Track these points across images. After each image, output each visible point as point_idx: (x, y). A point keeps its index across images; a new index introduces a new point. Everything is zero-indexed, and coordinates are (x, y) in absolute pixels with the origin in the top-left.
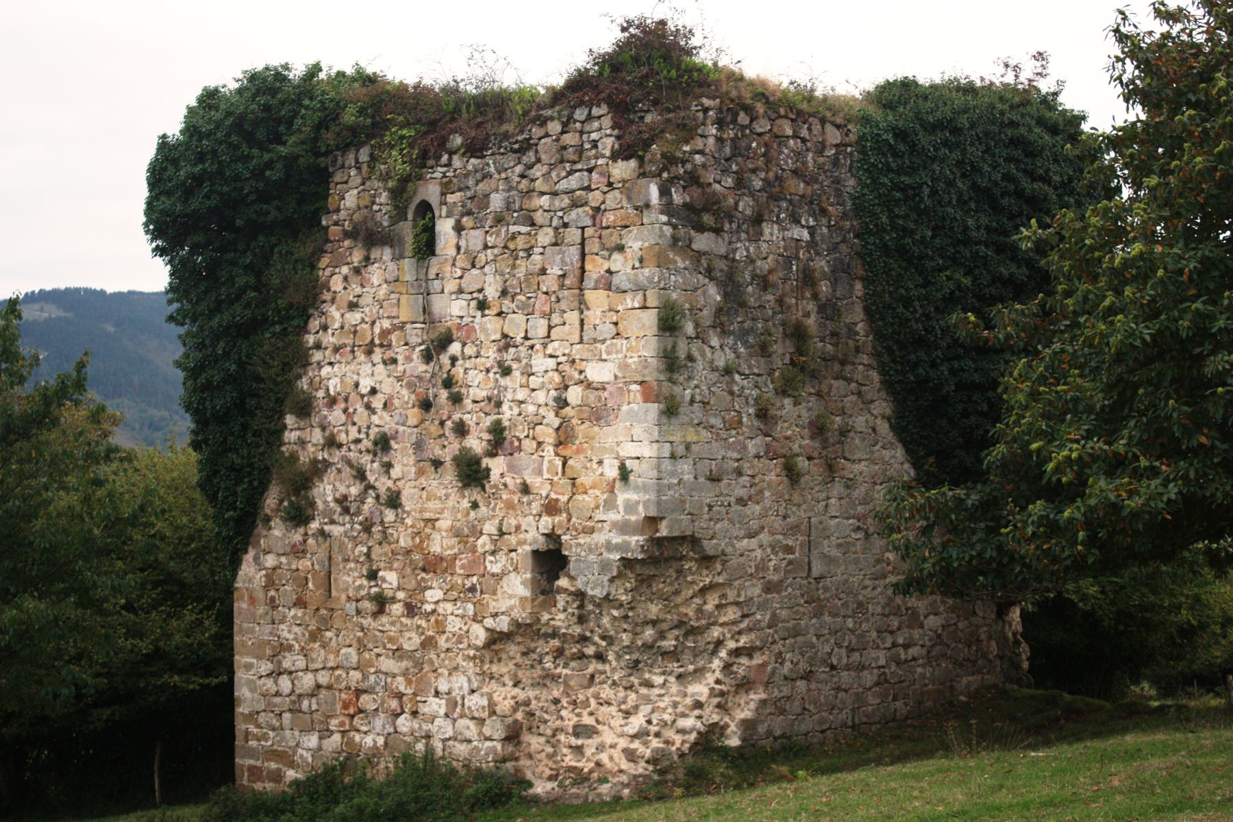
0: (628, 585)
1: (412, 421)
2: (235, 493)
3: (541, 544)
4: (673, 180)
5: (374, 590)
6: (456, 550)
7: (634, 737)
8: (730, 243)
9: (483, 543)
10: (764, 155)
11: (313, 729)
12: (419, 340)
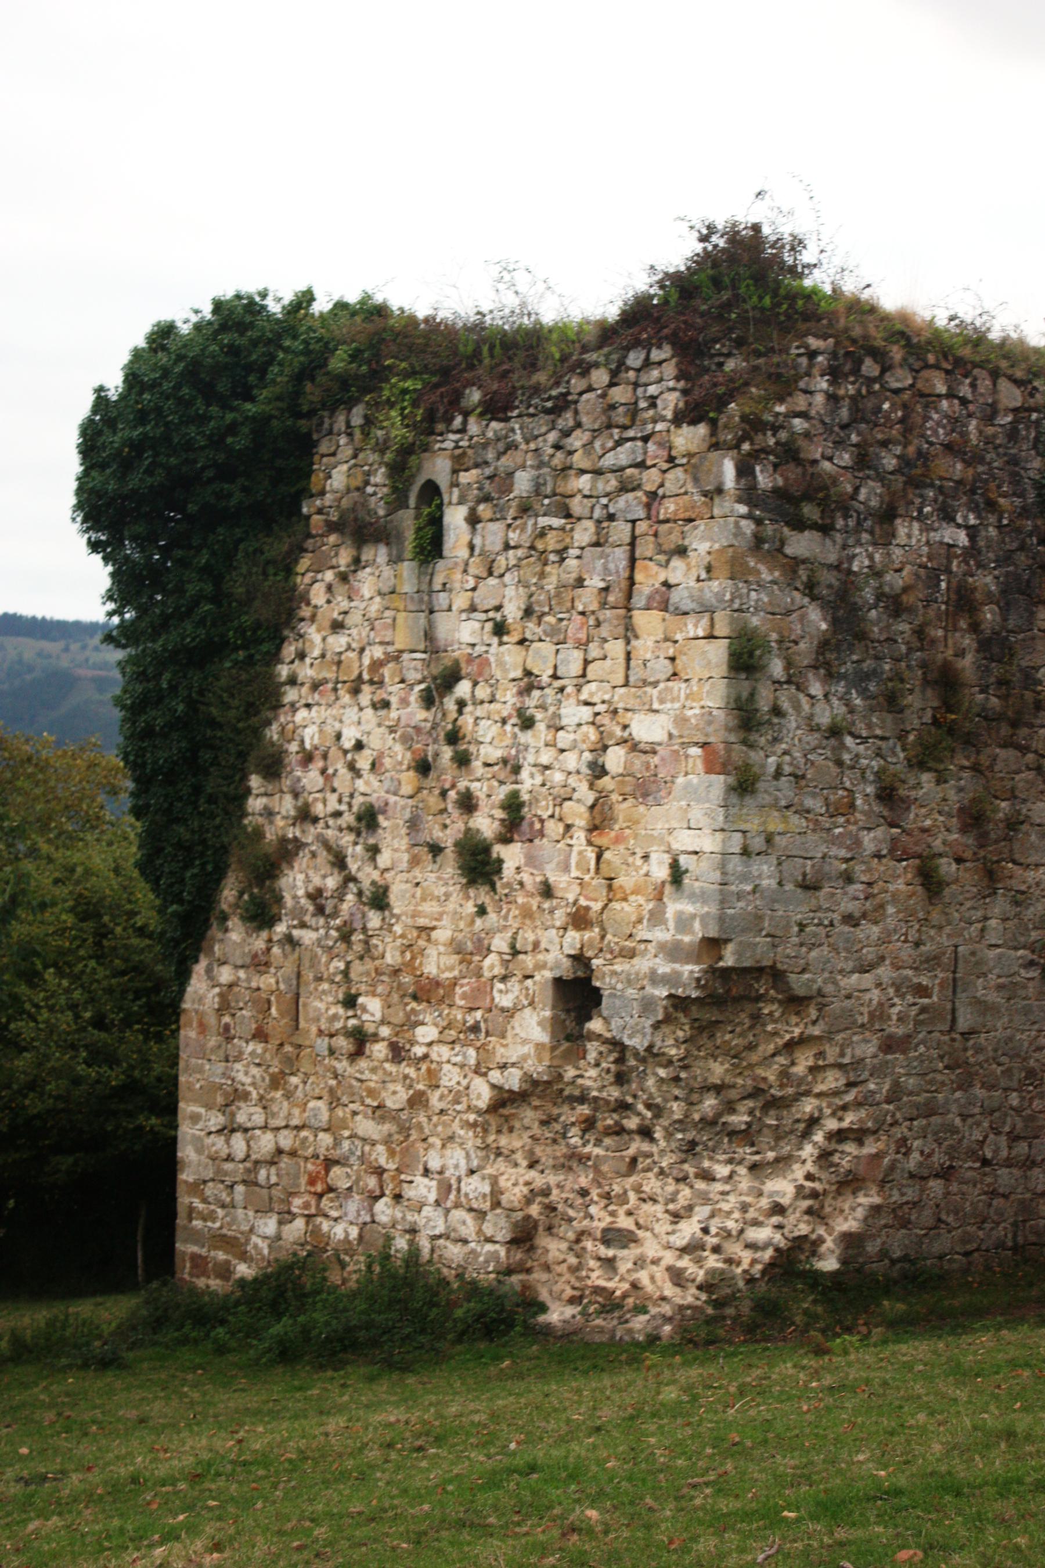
0: (680, 1034)
1: (407, 789)
2: (182, 881)
3: (566, 970)
4: (756, 455)
5: (352, 1022)
6: (456, 973)
7: (684, 1250)
8: (845, 547)
9: (491, 964)
10: (902, 421)
11: (271, 1210)
12: (419, 676)
